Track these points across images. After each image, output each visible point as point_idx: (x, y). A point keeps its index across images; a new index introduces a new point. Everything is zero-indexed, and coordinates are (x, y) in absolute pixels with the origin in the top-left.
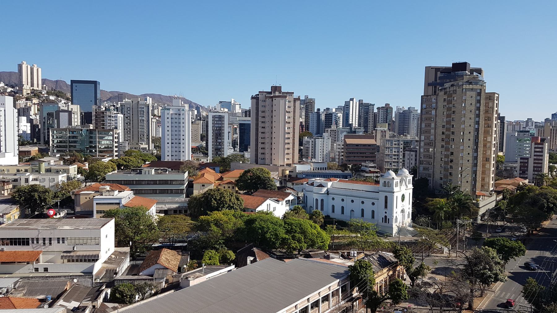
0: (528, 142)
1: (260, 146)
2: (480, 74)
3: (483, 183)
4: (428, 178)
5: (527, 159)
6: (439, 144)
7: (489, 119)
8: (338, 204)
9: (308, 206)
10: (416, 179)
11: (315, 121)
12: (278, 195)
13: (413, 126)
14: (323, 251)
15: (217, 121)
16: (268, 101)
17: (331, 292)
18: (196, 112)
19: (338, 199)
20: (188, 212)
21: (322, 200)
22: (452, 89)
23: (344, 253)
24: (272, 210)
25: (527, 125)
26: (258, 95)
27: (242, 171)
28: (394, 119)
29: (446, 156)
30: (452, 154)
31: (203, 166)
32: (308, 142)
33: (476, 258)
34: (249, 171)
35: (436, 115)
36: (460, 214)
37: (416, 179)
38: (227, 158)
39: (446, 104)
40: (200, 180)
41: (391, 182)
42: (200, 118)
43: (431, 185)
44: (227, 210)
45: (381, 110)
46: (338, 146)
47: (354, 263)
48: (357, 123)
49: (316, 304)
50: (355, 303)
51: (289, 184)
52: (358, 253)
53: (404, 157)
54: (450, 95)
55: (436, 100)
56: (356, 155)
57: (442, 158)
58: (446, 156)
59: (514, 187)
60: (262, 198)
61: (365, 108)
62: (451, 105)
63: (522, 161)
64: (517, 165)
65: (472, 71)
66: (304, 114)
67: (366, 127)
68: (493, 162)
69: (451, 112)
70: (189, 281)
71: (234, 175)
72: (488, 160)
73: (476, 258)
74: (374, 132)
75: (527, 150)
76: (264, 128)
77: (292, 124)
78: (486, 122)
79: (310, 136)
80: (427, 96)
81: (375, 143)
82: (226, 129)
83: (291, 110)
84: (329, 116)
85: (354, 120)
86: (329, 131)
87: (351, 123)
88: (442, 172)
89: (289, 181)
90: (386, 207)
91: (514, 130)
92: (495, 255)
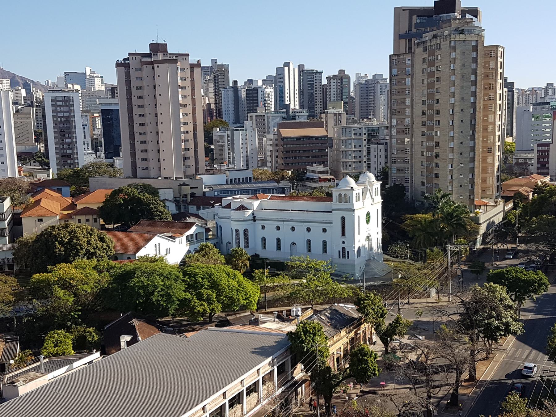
0: (548, 119)
1: (139, 147)
2: (476, 17)
3: (484, 185)
4: (405, 185)
5: (548, 145)
6: (418, 130)
7: (491, 88)
8: (271, 235)
9: (225, 243)
10: (387, 186)
11: (231, 102)
12: (173, 227)
13: (382, 101)
14: (249, 313)
15: (60, 107)
16: (147, 69)
17: (260, 377)
18: (23, 93)
19: (271, 226)
20: (16, 268)
21: (246, 231)
22: (434, 42)
23: (282, 312)
24: (163, 253)
25: (546, 94)
26: (128, 59)
27: (109, 192)
28: (353, 95)
29: (429, 149)
30: (437, 144)
31: (37, 188)
32: (222, 137)
33: (476, 303)
34: (120, 191)
35: (412, 85)
36: (451, 236)
37: (387, 186)
38: (81, 170)
39: (426, 67)
40: (34, 211)
41: (349, 195)
42: (32, 102)
43: (408, 194)
44: (85, 259)
45: (332, 81)
46: (269, 140)
47: (295, 328)
48: (297, 103)
49: (237, 400)
50: (299, 389)
51: (192, 209)
52: (304, 310)
53: (369, 153)
54: (432, 53)
55: (412, 60)
56: (297, 154)
57: (423, 152)
58: (429, 149)
59: (529, 189)
60: (144, 236)
61: (309, 79)
62: (434, 69)
63: (540, 148)
64: (533, 156)
65: (464, 12)
66: (211, 90)
67: (311, 109)
68: (498, 154)
69: (433, 79)
70: (17, 387)
71: (95, 199)
72: (490, 150)
73: (476, 303)
74: (323, 115)
75: (547, 132)
76: (143, 115)
77: (190, 108)
78: (486, 92)
79: (225, 126)
80: (398, 55)
81: (325, 134)
82: (79, 121)
83: (188, 83)
84: (253, 93)
85: (292, 99)
86: (254, 118)
87: (287, 103)
88: (425, 174)
89: (192, 203)
90: (343, 234)
91: (528, 102)
92: (504, 295)
